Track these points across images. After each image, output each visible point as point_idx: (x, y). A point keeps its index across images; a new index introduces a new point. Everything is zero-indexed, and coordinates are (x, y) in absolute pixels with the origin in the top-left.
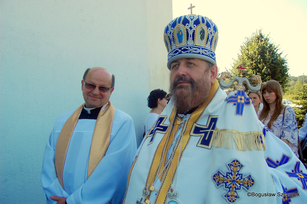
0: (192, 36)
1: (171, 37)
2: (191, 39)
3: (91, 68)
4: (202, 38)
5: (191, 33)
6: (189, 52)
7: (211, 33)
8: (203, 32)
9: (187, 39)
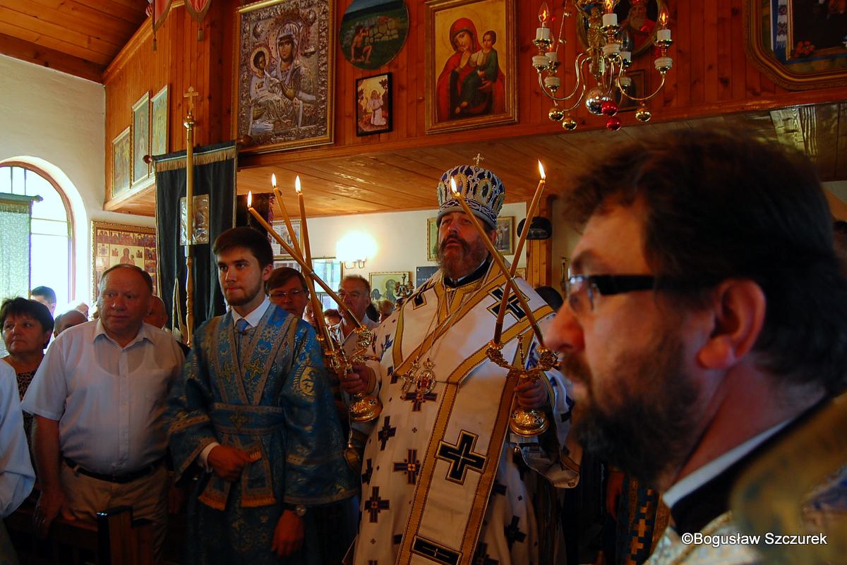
2: (471, 192)
3: (88, 216)
4: (484, 194)
5: (472, 186)
7: (496, 192)
8: (486, 188)
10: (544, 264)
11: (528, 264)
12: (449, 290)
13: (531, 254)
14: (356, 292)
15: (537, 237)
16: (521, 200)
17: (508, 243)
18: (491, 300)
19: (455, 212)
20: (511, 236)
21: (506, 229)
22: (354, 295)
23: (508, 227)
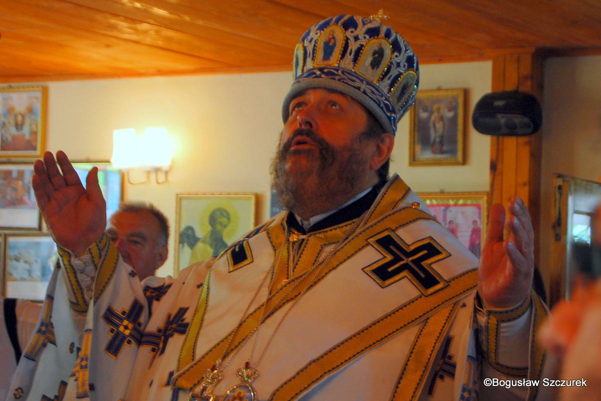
0: (353, 53)
1: (310, 49)
2: (349, 58)
4: (375, 64)
5: (353, 46)
6: (384, 98)
9: (343, 55)
10: (525, 184)
11: (492, 185)
12: (295, 238)
13: (499, 166)
14: (138, 235)
15: (512, 131)
16: (481, 57)
17: (454, 142)
18: (372, 256)
19: (315, 88)
20: (460, 127)
21: (450, 114)
22: (135, 242)
23: (453, 108)
